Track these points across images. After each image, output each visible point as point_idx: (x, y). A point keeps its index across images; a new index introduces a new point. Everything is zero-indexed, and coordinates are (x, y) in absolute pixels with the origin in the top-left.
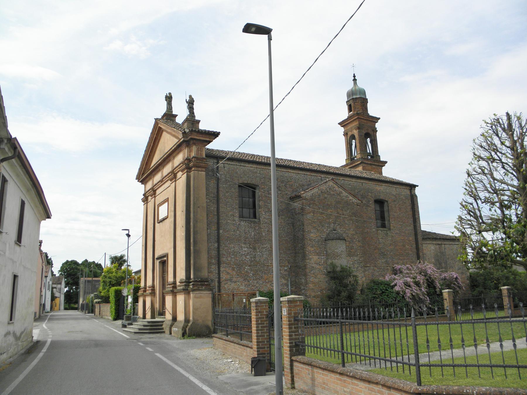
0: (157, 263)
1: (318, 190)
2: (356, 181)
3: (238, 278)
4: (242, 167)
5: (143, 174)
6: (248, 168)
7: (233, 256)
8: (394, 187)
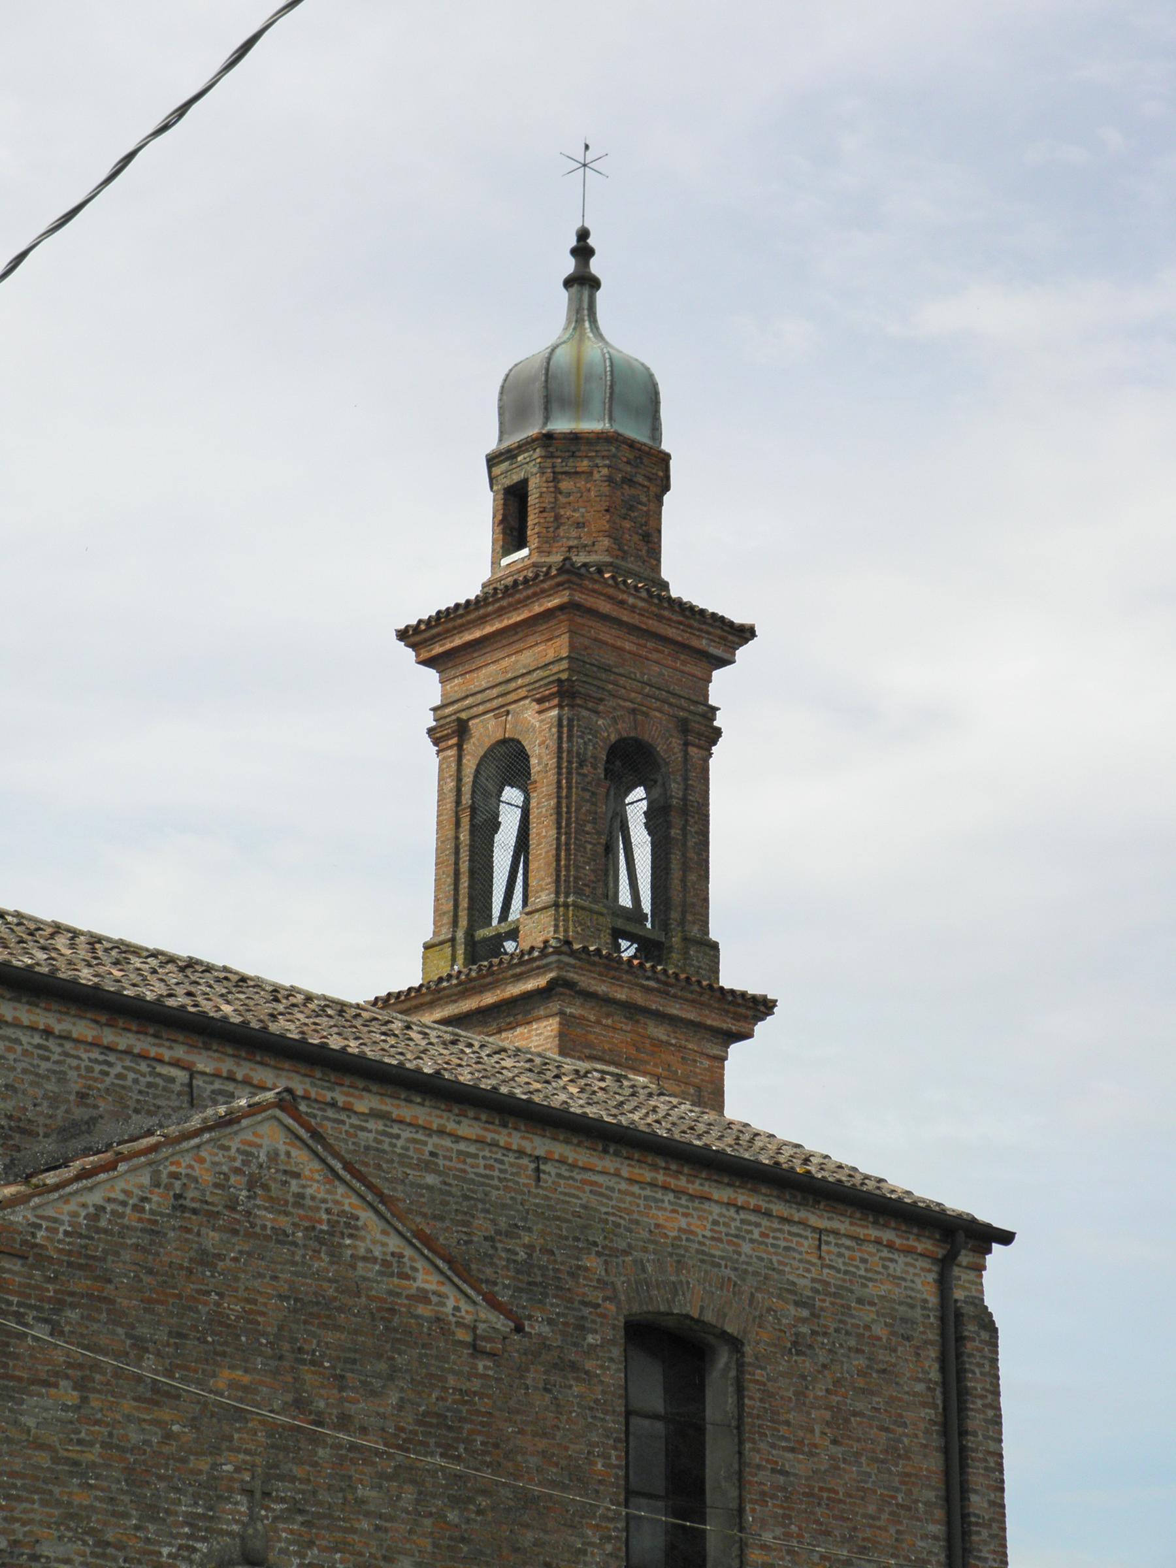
2: (489, 1136)
8: (802, 1223)
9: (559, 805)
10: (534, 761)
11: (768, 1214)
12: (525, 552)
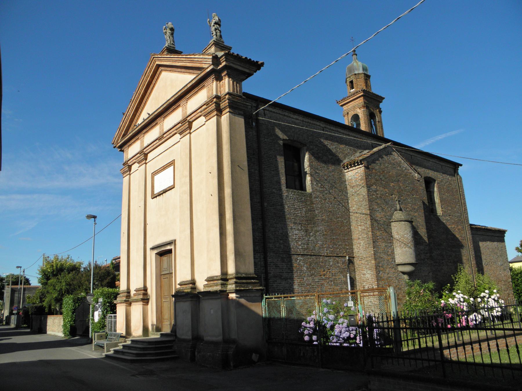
0: (152, 256)
1: (378, 156)
2: (406, 152)
3: (289, 273)
4: (286, 117)
5: (124, 135)
6: (293, 120)
7: (282, 241)
8: (440, 164)
9: (365, 122)
10: (360, 116)
11: (436, 163)
12: (354, 89)
